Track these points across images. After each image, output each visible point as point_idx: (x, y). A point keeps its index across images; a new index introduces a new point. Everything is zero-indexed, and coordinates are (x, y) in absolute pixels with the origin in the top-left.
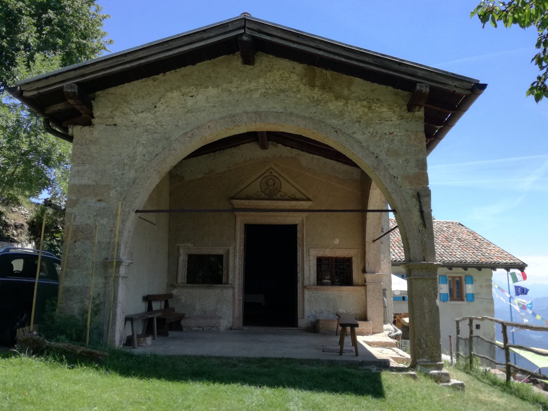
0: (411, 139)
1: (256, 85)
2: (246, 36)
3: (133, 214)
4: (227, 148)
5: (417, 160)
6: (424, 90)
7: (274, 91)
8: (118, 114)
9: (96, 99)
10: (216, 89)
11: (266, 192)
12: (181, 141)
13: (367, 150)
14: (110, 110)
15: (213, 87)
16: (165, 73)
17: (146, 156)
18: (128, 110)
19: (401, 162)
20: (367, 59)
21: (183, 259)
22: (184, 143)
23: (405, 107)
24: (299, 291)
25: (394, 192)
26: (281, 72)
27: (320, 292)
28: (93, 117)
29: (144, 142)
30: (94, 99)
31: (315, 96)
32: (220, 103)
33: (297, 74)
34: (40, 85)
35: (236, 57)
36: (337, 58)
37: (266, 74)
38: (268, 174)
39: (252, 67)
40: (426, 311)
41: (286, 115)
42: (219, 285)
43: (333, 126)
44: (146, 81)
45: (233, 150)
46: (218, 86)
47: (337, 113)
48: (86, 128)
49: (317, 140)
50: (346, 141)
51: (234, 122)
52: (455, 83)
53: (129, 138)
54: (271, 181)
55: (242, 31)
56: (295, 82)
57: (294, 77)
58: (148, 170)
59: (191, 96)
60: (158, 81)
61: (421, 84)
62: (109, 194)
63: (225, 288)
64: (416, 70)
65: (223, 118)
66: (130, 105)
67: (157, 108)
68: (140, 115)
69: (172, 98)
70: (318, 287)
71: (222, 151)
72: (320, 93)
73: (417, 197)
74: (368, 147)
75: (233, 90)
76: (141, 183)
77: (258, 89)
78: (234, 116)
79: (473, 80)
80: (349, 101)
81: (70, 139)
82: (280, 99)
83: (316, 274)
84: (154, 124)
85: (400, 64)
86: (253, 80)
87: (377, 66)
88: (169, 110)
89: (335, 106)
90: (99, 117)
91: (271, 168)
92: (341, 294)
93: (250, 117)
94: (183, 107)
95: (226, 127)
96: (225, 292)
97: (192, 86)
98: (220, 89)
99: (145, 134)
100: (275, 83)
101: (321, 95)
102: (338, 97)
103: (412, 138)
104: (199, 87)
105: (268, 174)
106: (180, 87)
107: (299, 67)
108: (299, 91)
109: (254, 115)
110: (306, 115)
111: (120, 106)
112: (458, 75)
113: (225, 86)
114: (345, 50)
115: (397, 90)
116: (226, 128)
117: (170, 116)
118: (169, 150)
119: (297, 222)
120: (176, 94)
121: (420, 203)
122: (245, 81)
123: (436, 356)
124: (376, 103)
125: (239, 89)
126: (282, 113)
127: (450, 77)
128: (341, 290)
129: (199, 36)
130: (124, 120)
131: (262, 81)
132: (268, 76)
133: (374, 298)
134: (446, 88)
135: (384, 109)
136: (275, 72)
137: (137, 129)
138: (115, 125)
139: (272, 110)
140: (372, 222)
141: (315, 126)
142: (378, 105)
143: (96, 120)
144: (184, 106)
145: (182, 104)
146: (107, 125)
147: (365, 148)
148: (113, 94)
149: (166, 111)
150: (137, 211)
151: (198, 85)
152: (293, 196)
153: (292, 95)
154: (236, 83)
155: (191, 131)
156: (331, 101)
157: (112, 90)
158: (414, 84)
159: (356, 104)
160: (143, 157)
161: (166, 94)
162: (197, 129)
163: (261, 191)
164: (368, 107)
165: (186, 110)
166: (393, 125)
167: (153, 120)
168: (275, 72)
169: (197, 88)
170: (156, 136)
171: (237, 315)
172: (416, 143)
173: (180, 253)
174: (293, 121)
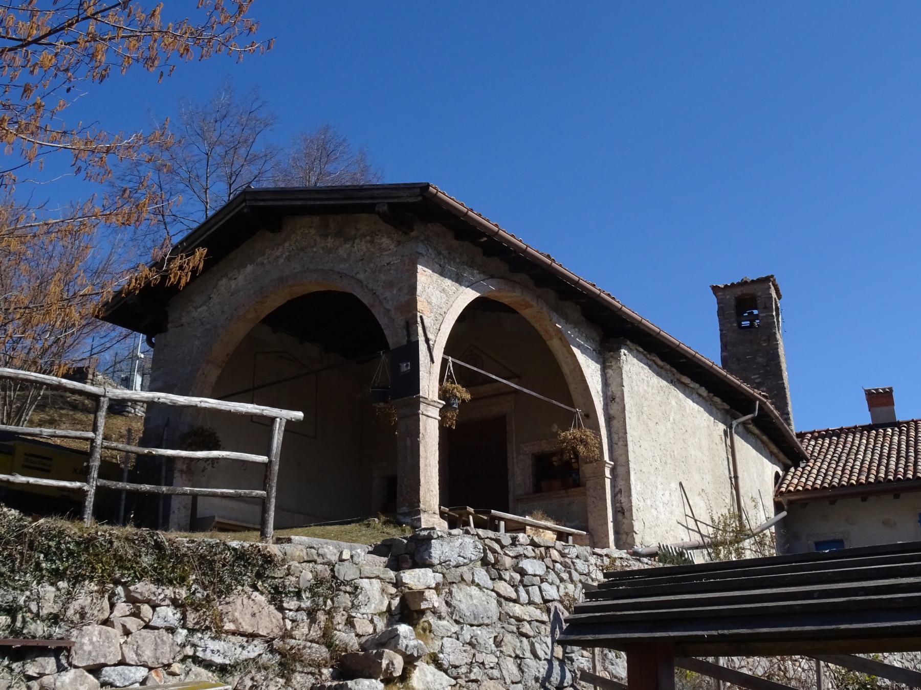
20: (335, 196)
36: (309, 203)
55: (244, 204)
72: (333, 240)
75: (265, 262)
102: (346, 241)
107: (316, 219)
120: (224, 281)
127: (403, 188)
131: (287, 244)
133: (596, 498)
134: (401, 200)
135: (384, 240)
140: (576, 388)
142: (379, 237)
158: (374, 205)
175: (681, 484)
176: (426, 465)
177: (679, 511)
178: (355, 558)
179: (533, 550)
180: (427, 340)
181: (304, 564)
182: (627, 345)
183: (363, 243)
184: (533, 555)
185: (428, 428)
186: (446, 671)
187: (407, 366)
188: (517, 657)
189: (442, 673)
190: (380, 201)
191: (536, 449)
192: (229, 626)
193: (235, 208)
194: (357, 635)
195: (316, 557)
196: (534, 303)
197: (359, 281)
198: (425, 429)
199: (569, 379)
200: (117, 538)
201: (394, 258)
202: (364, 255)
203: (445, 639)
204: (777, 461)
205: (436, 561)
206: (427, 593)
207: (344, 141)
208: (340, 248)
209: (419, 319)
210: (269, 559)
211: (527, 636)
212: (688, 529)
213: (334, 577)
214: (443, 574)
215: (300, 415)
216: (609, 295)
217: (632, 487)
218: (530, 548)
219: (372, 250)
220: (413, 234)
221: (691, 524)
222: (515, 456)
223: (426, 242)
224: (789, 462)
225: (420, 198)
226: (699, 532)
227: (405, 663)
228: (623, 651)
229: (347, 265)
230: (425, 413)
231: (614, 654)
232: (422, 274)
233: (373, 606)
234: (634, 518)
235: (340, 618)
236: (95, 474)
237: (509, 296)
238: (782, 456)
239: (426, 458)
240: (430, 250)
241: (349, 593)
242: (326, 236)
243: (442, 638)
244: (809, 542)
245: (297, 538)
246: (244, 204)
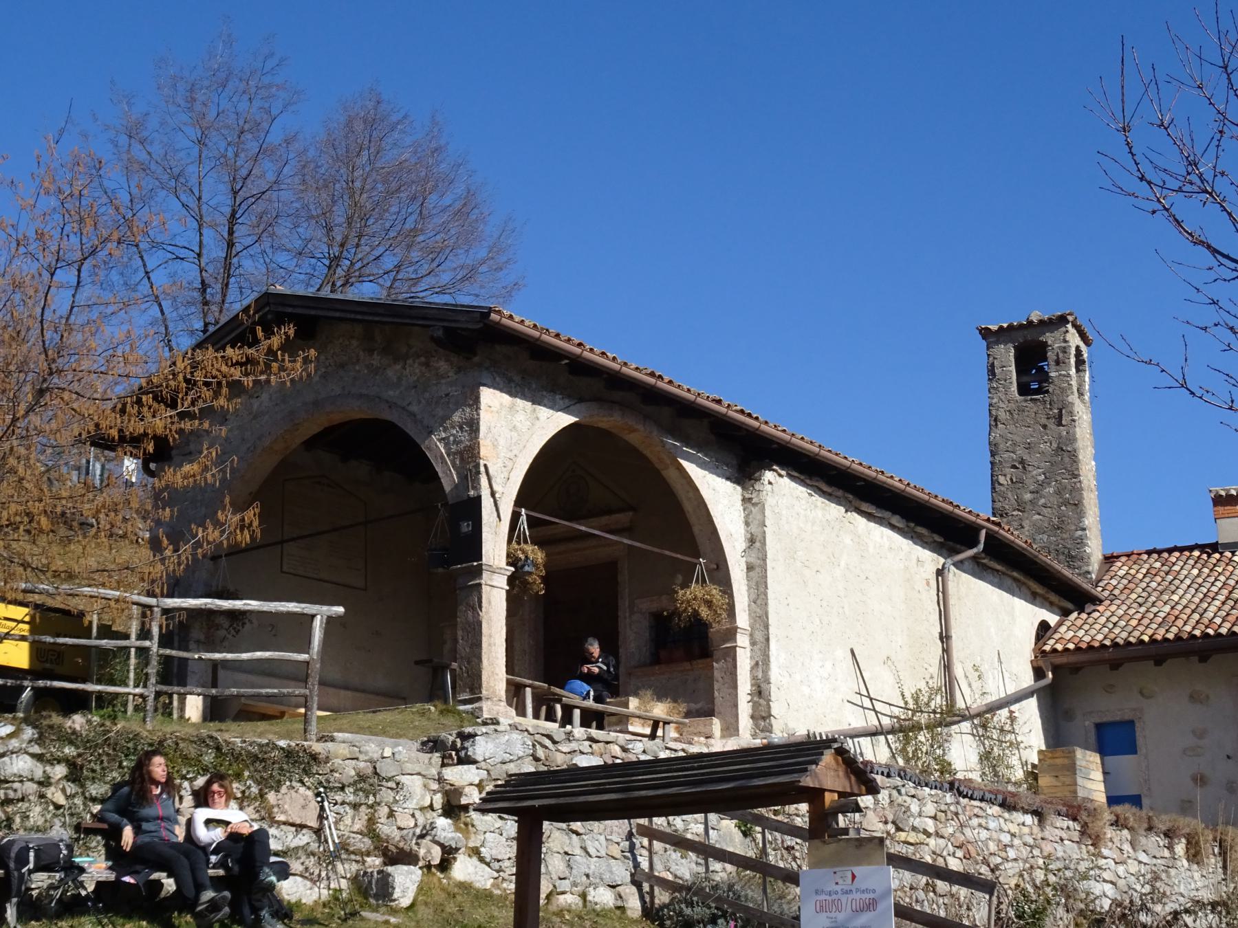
55: (267, 309)
102: (396, 359)
175: (852, 652)
176: (490, 645)
177: (848, 685)
178: (396, 756)
179: (590, 746)
180: (493, 494)
181: (347, 762)
182: (774, 470)
183: (416, 365)
184: (590, 750)
185: (492, 599)
186: (488, 864)
187: (468, 525)
188: (566, 853)
189: (484, 866)
191: (655, 607)
192: (282, 818)
194: (399, 828)
195: (358, 755)
196: (640, 427)
197: (413, 415)
198: (490, 603)
199: (693, 519)
200: (182, 739)
201: (454, 388)
203: (488, 834)
204: (1048, 604)
205: (480, 758)
206: (467, 790)
207: (405, 117)
209: (482, 469)
210: (314, 757)
211: (578, 834)
212: (864, 708)
213: (376, 773)
214: (488, 771)
215: (340, 610)
216: (742, 412)
217: (772, 659)
218: (587, 743)
219: (427, 375)
220: (476, 359)
221: (867, 703)
222: (627, 614)
223: (492, 369)
224: (1070, 606)
225: (481, 325)
226: (876, 712)
227: (443, 853)
228: (692, 851)
229: (397, 392)
230: (489, 583)
231: (679, 855)
232: (486, 411)
233: (415, 801)
234: (772, 699)
235: (384, 811)
236: (153, 680)
237: (609, 420)
238: (1053, 597)
239: (490, 636)
240: (497, 379)
241: (392, 789)
242: (371, 351)
243: (485, 833)
244: (1087, 723)
245: (340, 735)
246: (267, 309)
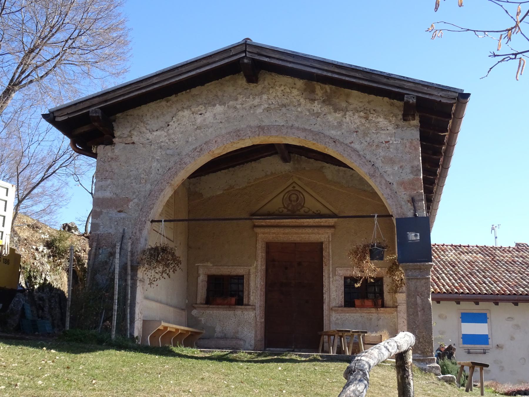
0: (406, 147)
1: (259, 101)
2: (247, 59)
3: (149, 223)
4: (247, 162)
5: (412, 167)
6: (411, 101)
7: (277, 106)
8: (135, 133)
9: (117, 120)
10: (223, 106)
11: (289, 208)
12: (190, 156)
13: (364, 158)
14: (129, 130)
15: (220, 105)
16: (177, 94)
17: (160, 171)
18: (144, 129)
19: (396, 169)
20: (357, 75)
21: (202, 279)
22: (193, 157)
23: (401, 117)
24: (326, 312)
25: (390, 197)
26: (283, 88)
27: (348, 315)
28: (114, 137)
29: (158, 158)
30: (114, 121)
31: (315, 109)
32: (226, 119)
33: (298, 89)
34: (69, 111)
35: (241, 77)
37: (268, 90)
38: (290, 188)
39: (255, 84)
40: (419, 309)
41: (287, 128)
42: (240, 307)
43: (332, 137)
44: (161, 102)
45: (253, 164)
46: (224, 104)
47: (336, 124)
48: (108, 147)
49: (319, 150)
50: (345, 151)
51: (239, 136)
52: (441, 93)
53: (145, 155)
54: (294, 196)
55: (244, 55)
56: (296, 97)
57: (295, 92)
58: (162, 183)
59: (200, 114)
60: (171, 102)
61: (408, 96)
62: (127, 206)
63: (246, 310)
64: (404, 83)
65: (229, 133)
66: (146, 124)
67: (170, 126)
68: (155, 133)
69: (183, 116)
70: (346, 309)
71: (241, 165)
72: (320, 106)
73: (411, 201)
74: (365, 156)
75: (238, 106)
76: (156, 195)
77: (261, 104)
78: (239, 131)
79: (458, 89)
80: (347, 113)
81: (95, 156)
82: (281, 113)
83: (343, 296)
84: (167, 141)
85: (389, 77)
86: (257, 97)
87: (366, 80)
88: (181, 128)
89: (333, 118)
90: (120, 137)
91: (294, 182)
92: (370, 316)
93: (253, 131)
94: (193, 125)
95: (232, 141)
96: (246, 314)
97: (201, 105)
98: (227, 106)
99: (159, 150)
100: (277, 98)
101: (321, 108)
102: (336, 110)
103: (407, 146)
104: (207, 106)
105: (290, 188)
106: (191, 106)
107: (300, 83)
108: (300, 105)
109: (257, 129)
110: (306, 127)
111: (138, 126)
112: (443, 86)
113: (231, 103)
114: (337, 67)
115: (392, 101)
116: (231, 142)
117: (181, 133)
118: (180, 164)
119: (323, 240)
120: (186, 113)
121: (414, 207)
122: (249, 98)
123: (428, 351)
124: (372, 114)
125: (244, 106)
126: (283, 126)
127: (436, 88)
128: (370, 313)
129: (205, 62)
130: (141, 138)
131: (265, 97)
132: (271, 92)
135: (381, 119)
136: (277, 88)
137: (153, 147)
138: (133, 143)
139: (274, 124)
141: (314, 137)
142: (375, 115)
143: (117, 139)
144: (194, 123)
145: (192, 122)
146: (126, 144)
147: (362, 157)
148: (132, 115)
149: (177, 129)
150: (152, 221)
151: (206, 104)
152: (317, 211)
153: (293, 109)
154: (241, 100)
155: (200, 146)
156: (330, 113)
157: (130, 112)
159: (354, 115)
160: (157, 171)
161: (178, 113)
162: (205, 144)
163: (283, 206)
164: (365, 118)
165: (196, 127)
166: (389, 134)
167: (166, 138)
168: (277, 88)
169: (205, 106)
170: (168, 152)
171: (259, 337)
172: (411, 151)
173: (199, 273)
174: (294, 133)
187: (416, 236)
190: (407, 92)
191: (348, 274)
193: (233, 56)
197: (355, 150)
202: (358, 127)
208: (328, 115)
242: (313, 100)
